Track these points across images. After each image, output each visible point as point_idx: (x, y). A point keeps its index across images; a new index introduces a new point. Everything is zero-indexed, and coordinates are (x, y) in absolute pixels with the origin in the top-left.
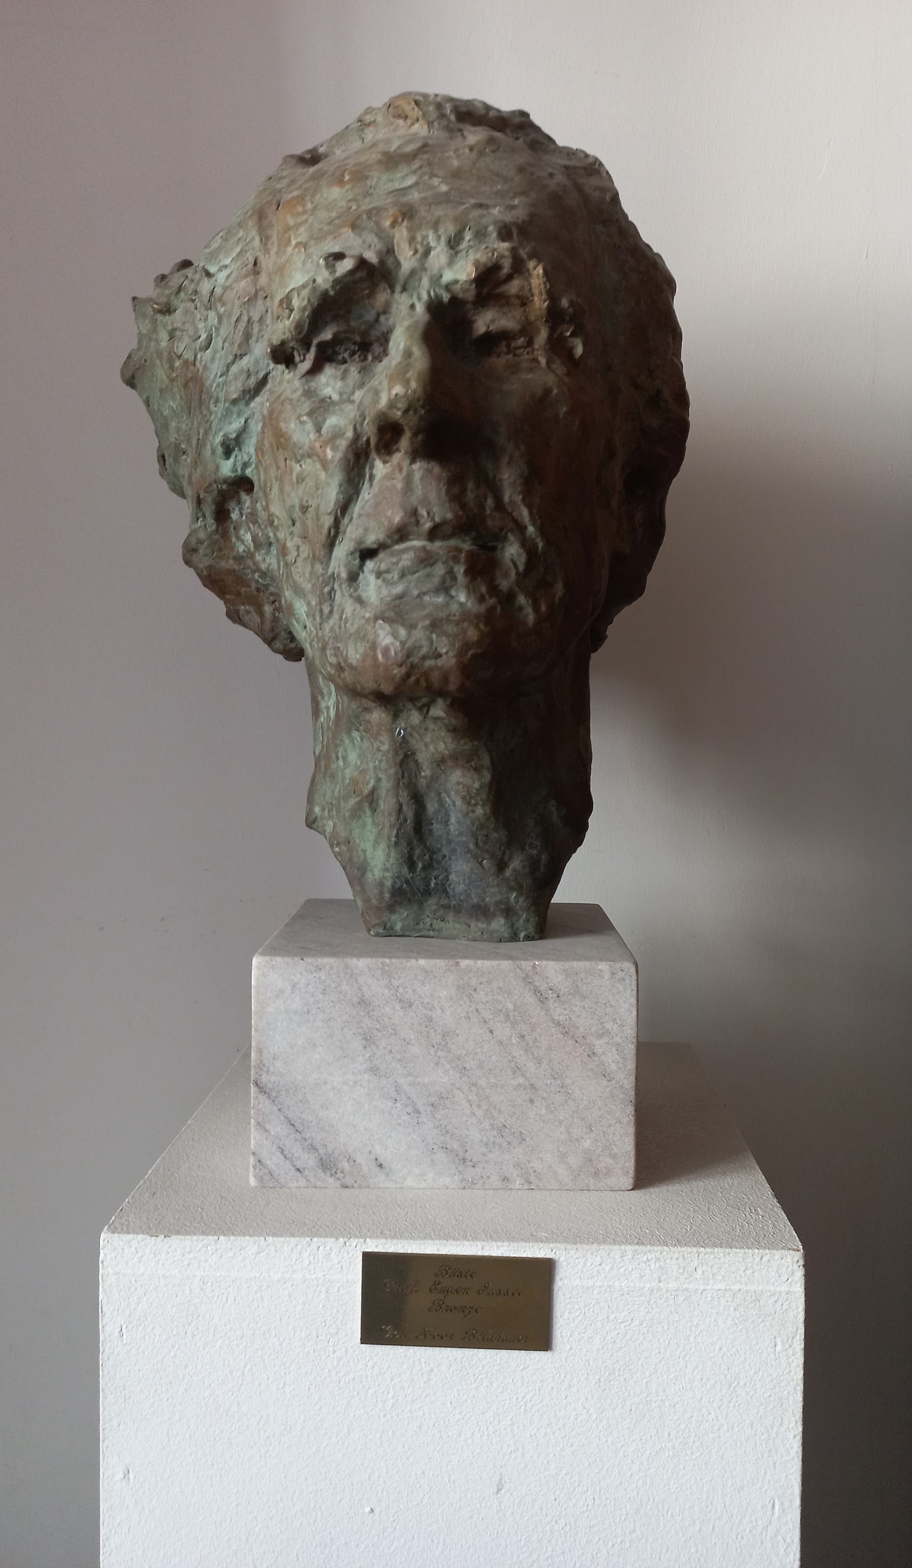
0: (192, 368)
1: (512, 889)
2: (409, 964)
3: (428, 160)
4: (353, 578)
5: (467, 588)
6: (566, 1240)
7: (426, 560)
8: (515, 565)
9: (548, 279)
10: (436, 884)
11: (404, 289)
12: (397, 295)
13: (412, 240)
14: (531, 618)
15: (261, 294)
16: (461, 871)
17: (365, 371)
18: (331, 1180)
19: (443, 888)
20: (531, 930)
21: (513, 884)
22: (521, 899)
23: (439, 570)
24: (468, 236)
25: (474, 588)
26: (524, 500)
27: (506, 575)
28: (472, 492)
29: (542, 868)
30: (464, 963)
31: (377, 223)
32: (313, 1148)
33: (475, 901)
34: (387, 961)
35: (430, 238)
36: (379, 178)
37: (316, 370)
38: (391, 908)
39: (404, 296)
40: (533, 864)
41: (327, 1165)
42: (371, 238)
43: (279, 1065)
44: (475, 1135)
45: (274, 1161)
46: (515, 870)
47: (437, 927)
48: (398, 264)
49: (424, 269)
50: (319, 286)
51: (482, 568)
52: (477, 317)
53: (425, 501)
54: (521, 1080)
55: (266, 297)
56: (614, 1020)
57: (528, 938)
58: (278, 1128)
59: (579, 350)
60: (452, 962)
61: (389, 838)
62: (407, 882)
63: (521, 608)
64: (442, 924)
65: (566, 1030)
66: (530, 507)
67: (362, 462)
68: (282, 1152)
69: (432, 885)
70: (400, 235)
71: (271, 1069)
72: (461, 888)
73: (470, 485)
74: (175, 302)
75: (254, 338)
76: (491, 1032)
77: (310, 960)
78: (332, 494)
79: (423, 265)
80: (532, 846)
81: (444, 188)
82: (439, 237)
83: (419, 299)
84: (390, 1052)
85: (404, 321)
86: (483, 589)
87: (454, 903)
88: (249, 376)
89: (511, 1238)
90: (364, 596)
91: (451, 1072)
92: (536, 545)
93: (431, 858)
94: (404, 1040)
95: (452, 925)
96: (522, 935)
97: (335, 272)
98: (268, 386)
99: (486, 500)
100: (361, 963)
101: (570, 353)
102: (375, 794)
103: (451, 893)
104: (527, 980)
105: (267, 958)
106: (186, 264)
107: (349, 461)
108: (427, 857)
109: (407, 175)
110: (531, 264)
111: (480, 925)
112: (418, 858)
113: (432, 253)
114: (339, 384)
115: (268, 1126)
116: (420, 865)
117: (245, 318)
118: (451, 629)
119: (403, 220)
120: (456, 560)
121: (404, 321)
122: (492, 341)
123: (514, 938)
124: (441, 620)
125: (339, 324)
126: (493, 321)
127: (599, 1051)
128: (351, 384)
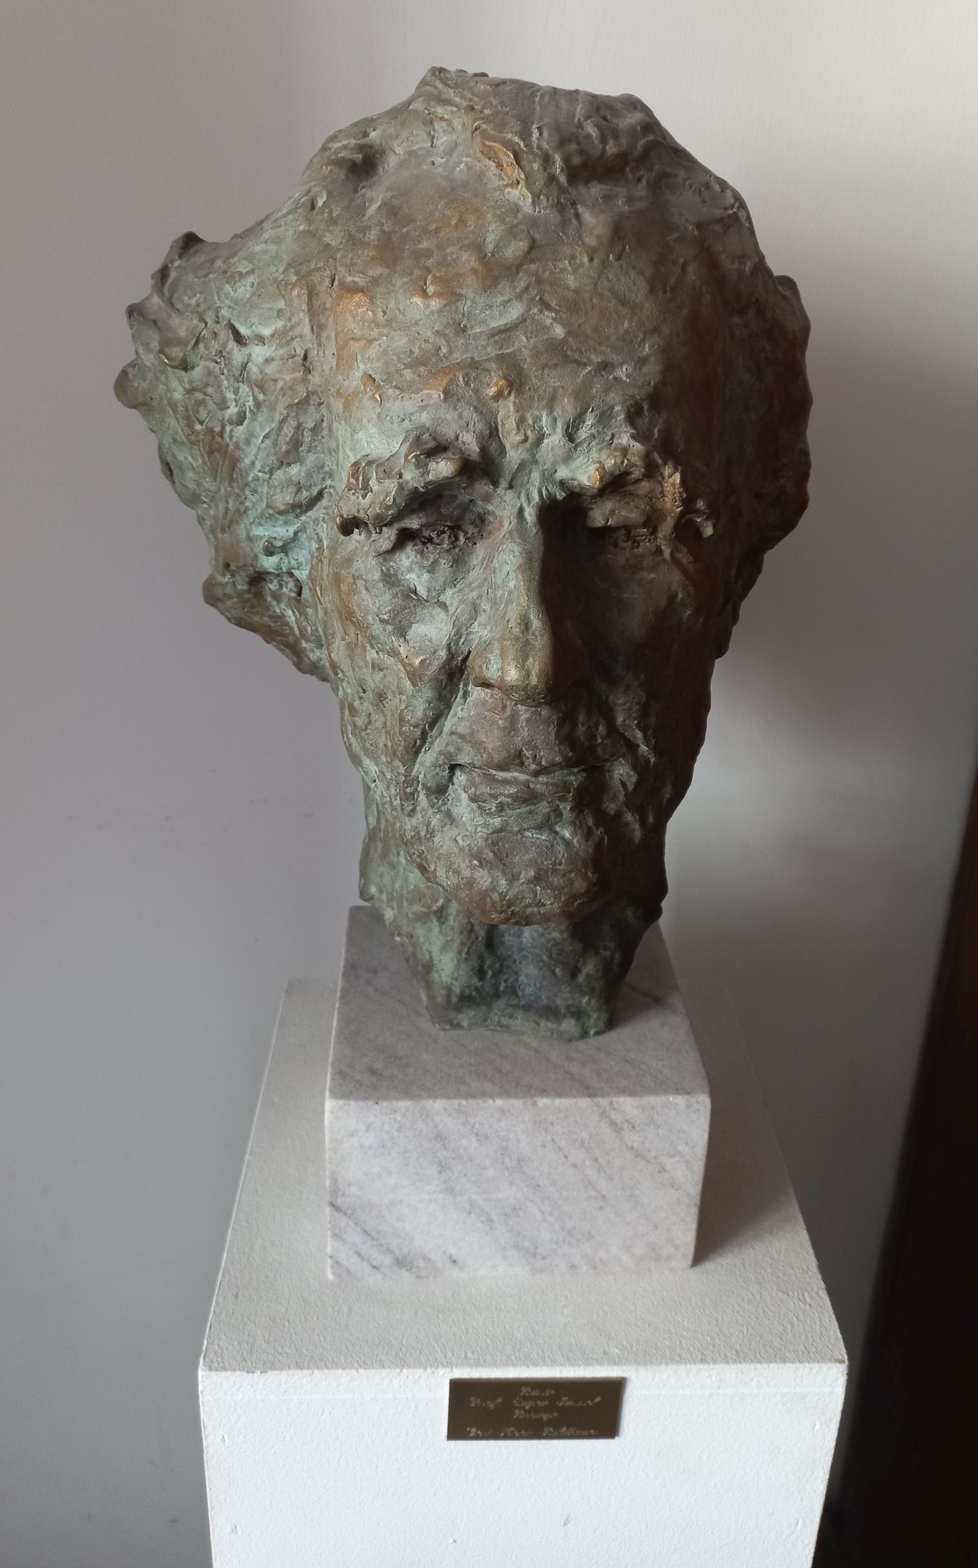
0: (219, 439)
1: (584, 994)
2: (486, 1105)
3: (537, 273)
4: (440, 790)
5: (573, 823)
6: (638, 1363)
7: (528, 797)
8: (624, 785)
9: (686, 490)
10: (506, 987)
11: (511, 487)
12: (500, 490)
13: (521, 422)
14: (638, 834)
15: (314, 400)
16: (530, 976)
17: (459, 562)
18: (407, 1274)
19: (513, 991)
20: (601, 1025)
21: (585, 989)
22: (593, 1001)
23: (544, 807)
24: (590, 420)
25: (580, 822)
26: (638, 725)
27: (614, 798)
28: (583, 725)
29: (615, 967)
30: (543, 1102)
31: (476, 392)
32: (389, 1251)
33: (546, 1002)
34: (464, 1102)
35: (544, 419)
36: (474, 301)
37: (399, 545)
38: (458, 1009)
39: (509, 496)
40: (606, 966)
41: (402, 1263)
42: (469, 414)
43: (354, 1189)
44: (546, 1236)
45: (350, 1261)
46: (588, 975)
47: (505, 1023)
48: (502, 450)
49: (536, 462)
50: (407, 483)
51: (589, 799)
52: (594, 506)
53: (530, 743)
54: (593, 1193)
55: (320, 404)
56: (687, 1144)
57: (598, 1033)
58: (355, 1237)
59: (708, 531)
60: (529, 1102)
61: (460, 953)
62: (477, 990)
63: (627, 824)
64: (510, 1021)
65: (640, 1155)
66: (644, 730)
67: (455, 680)
68: (359, 1255)
69: (502, 989)
70: (507, 412)
71: (347, 1193)
72: (529, 990)
73: (581, 717)
74: (193, 358)
75: (304, 448)
76: (566, 1157)
77: (385, 1104)
78: (420, 708)
79: (534, 456)
80: (606, 948)
81: (559, 331)
82: (555, 420)
83: (529, 499)
84: (465, 1175)
85: (512, 511)
86: (590, 822)
87: (522, 1003)
88: (299, 490)
89: (587, 1363)
90: (455, 811)
91: (525, 1189)
92: (648, 761)
93: (502, 966)
94: (479, 1165)
95: (519, 1021)
96: (592, 1032)
97: (428, 473)
98: (324, 502)
99: (597, 729)
100: (438, 1105)
101: (698, 532)
102: (445, 911)
103: (520, 993)
104: (603, 1114)
105: (341, 1102)
106: (190, 242)
107: (441, 681)
108: (497, 966)
109: (510, 300)
110: (667, 471)
111: (550, 1024)
112: (489, 967)
113: (546, 441)
114: (426, 576)
115: (344, 1236)
116: (490, 973)
117: (293, 423)
118: (557, 881)
119: (509, 394)
120: (563, 799)
121: (512, 511)
122: (606, 531)
123: (584, 1034)
124: (546, 872)
125: (438, 514)
126: (612, 512)
127: (668, 1167)
128: (442, 579)
